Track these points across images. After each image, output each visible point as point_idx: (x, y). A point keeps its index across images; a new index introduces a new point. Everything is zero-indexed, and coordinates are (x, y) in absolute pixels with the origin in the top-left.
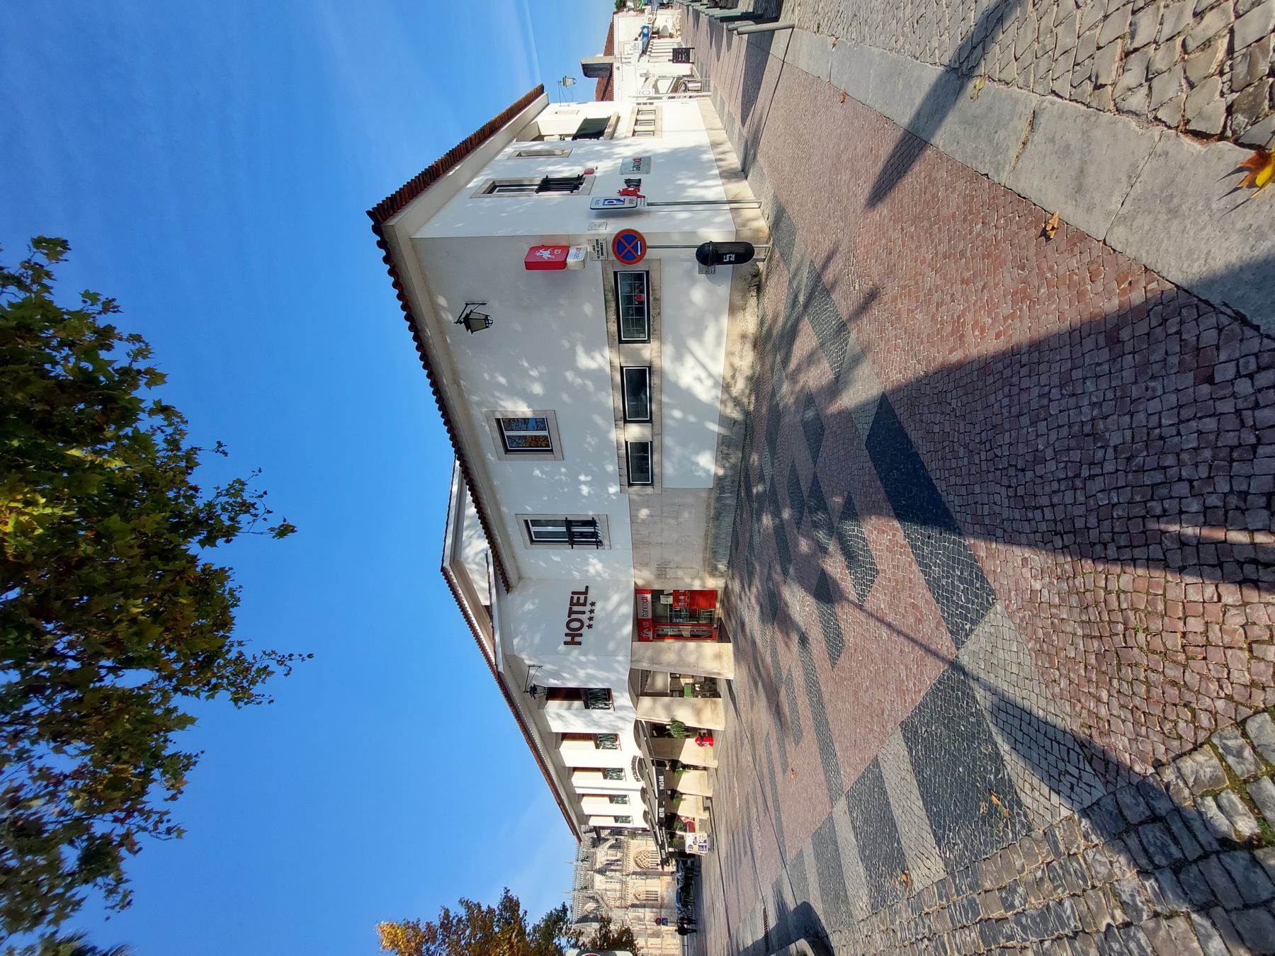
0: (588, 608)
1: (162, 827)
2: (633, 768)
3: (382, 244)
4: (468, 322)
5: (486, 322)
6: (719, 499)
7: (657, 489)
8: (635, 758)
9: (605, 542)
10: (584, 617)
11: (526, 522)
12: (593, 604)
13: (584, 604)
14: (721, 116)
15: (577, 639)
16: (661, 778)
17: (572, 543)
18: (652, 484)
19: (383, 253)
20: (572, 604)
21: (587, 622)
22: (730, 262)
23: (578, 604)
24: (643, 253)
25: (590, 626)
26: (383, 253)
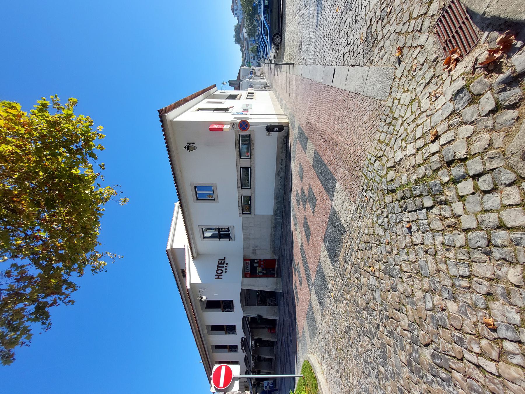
0: (225, 265)
1: (67, 300)
2: (241, 345)
3: (161, 121)
4: (188, 148)
5: (194, 148)
6: (275, 219)
7: (253, 215)
8: (242, 338)
9: (233, 238)
10: (223, 269)
11: (202, 229)
12: (227, 264)
13: (224, 264)
14: (276, 96)
15: (220, 277)
16: (253, 342)
17: (220, 238)
18: (251, 214)
19: (161, 124)
20: (219, 264)
21: (224, 271)
22: (276, 131)
23: (221, 264)
24: (249, 128)
25: (225, 272)
26: (161, 124)
